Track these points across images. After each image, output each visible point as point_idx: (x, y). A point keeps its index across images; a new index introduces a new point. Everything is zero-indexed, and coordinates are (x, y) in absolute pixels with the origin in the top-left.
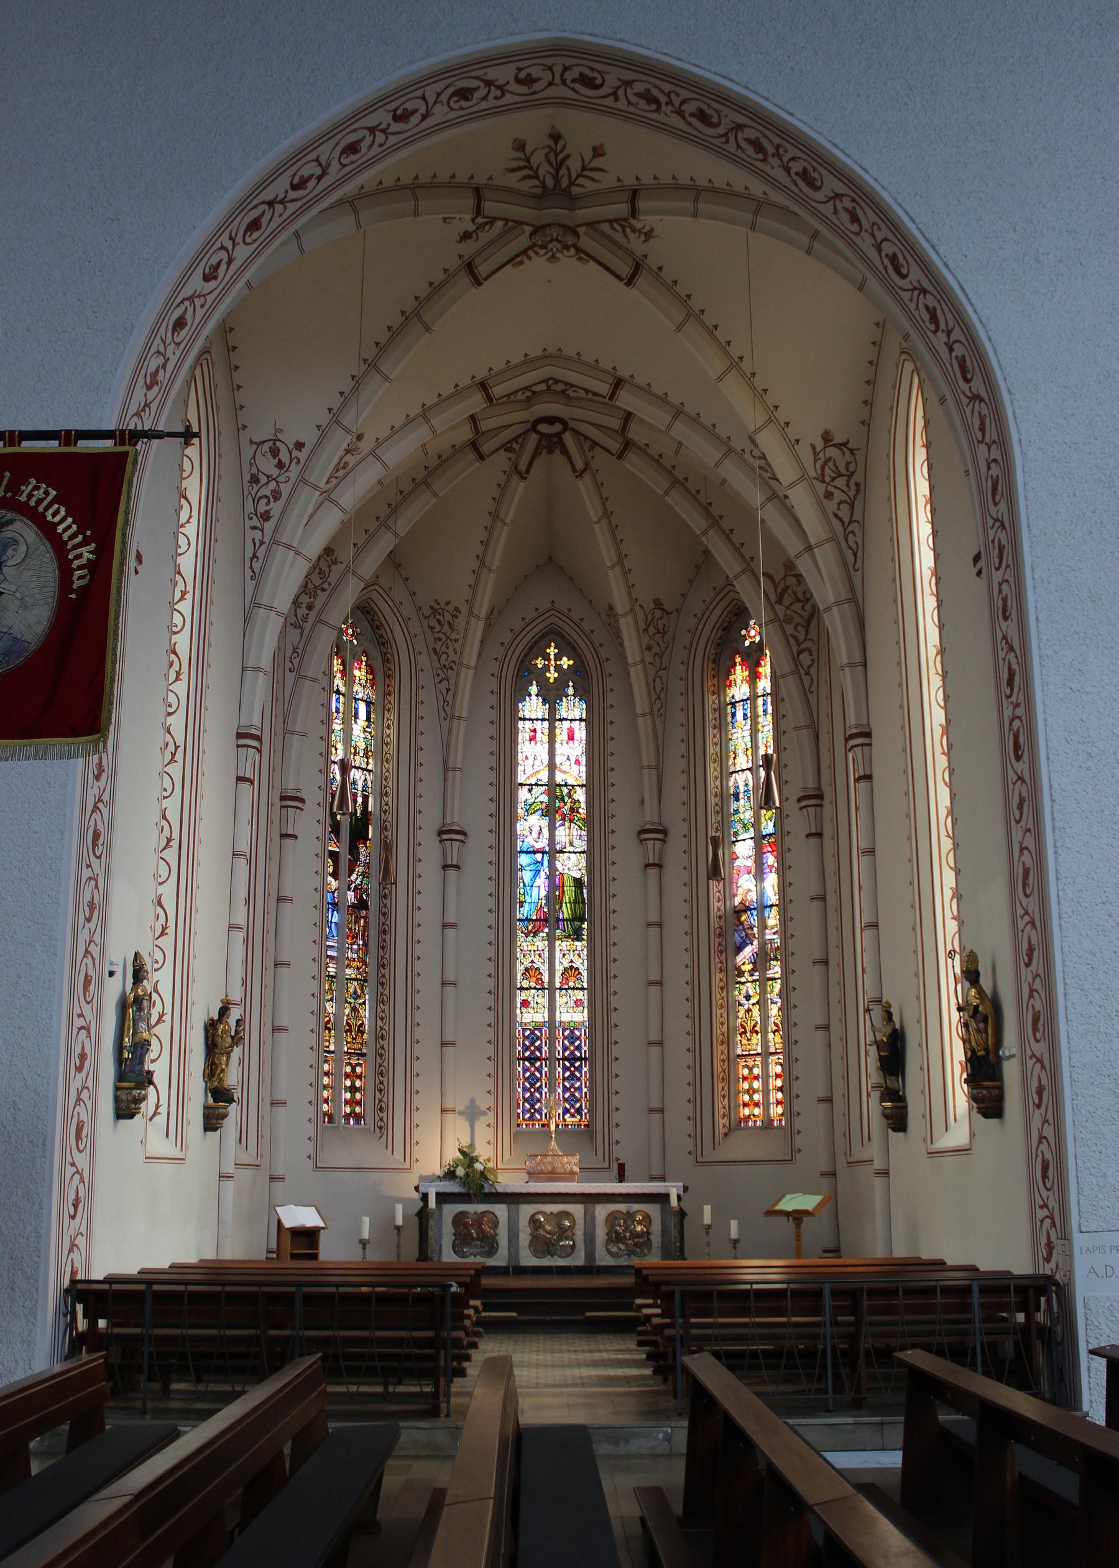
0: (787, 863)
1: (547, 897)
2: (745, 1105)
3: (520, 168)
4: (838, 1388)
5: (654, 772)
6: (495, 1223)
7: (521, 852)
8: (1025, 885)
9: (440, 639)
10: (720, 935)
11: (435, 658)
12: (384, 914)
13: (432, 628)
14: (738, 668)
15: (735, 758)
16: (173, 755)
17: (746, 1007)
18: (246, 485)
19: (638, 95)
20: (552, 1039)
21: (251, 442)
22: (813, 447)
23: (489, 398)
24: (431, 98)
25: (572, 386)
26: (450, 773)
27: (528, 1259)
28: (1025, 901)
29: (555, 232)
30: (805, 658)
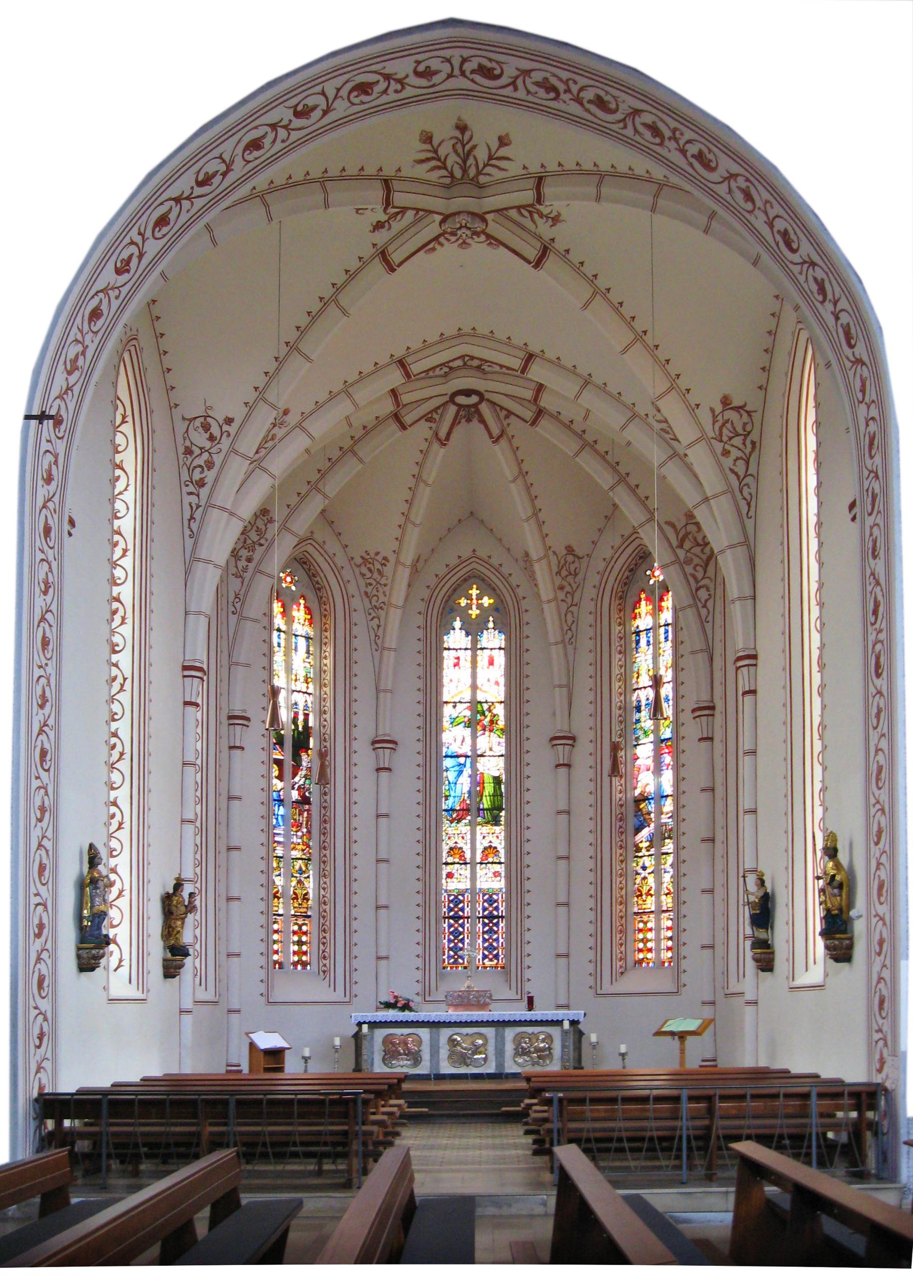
0: (681, 762)
1: (469, 792)
2: (640, 951)
3: (428, 160)
4: (691, 1167)
5: (565, 690)
6: (420, 1042)
7: (446, 756)
8: (878, 779)
9: (370, 584)
10: (621, 820)
11: (366, 601)
12: (325, 808)
13: (363, 575)
14: (643, 603)
15: (638, 678)
16: (122, 686)
17: (642, 876)
18: (181, 456)
19: (537, 84)
20: (473, 902)
21: (184, 419)
22: (712, 410)
23: (408, 375)
24: (331, 94)
25: (487, 361)
26: (382, 695)
27: (447, 1068)
28: (877, 792)
29: (463, 219)
30: (703, 594)
